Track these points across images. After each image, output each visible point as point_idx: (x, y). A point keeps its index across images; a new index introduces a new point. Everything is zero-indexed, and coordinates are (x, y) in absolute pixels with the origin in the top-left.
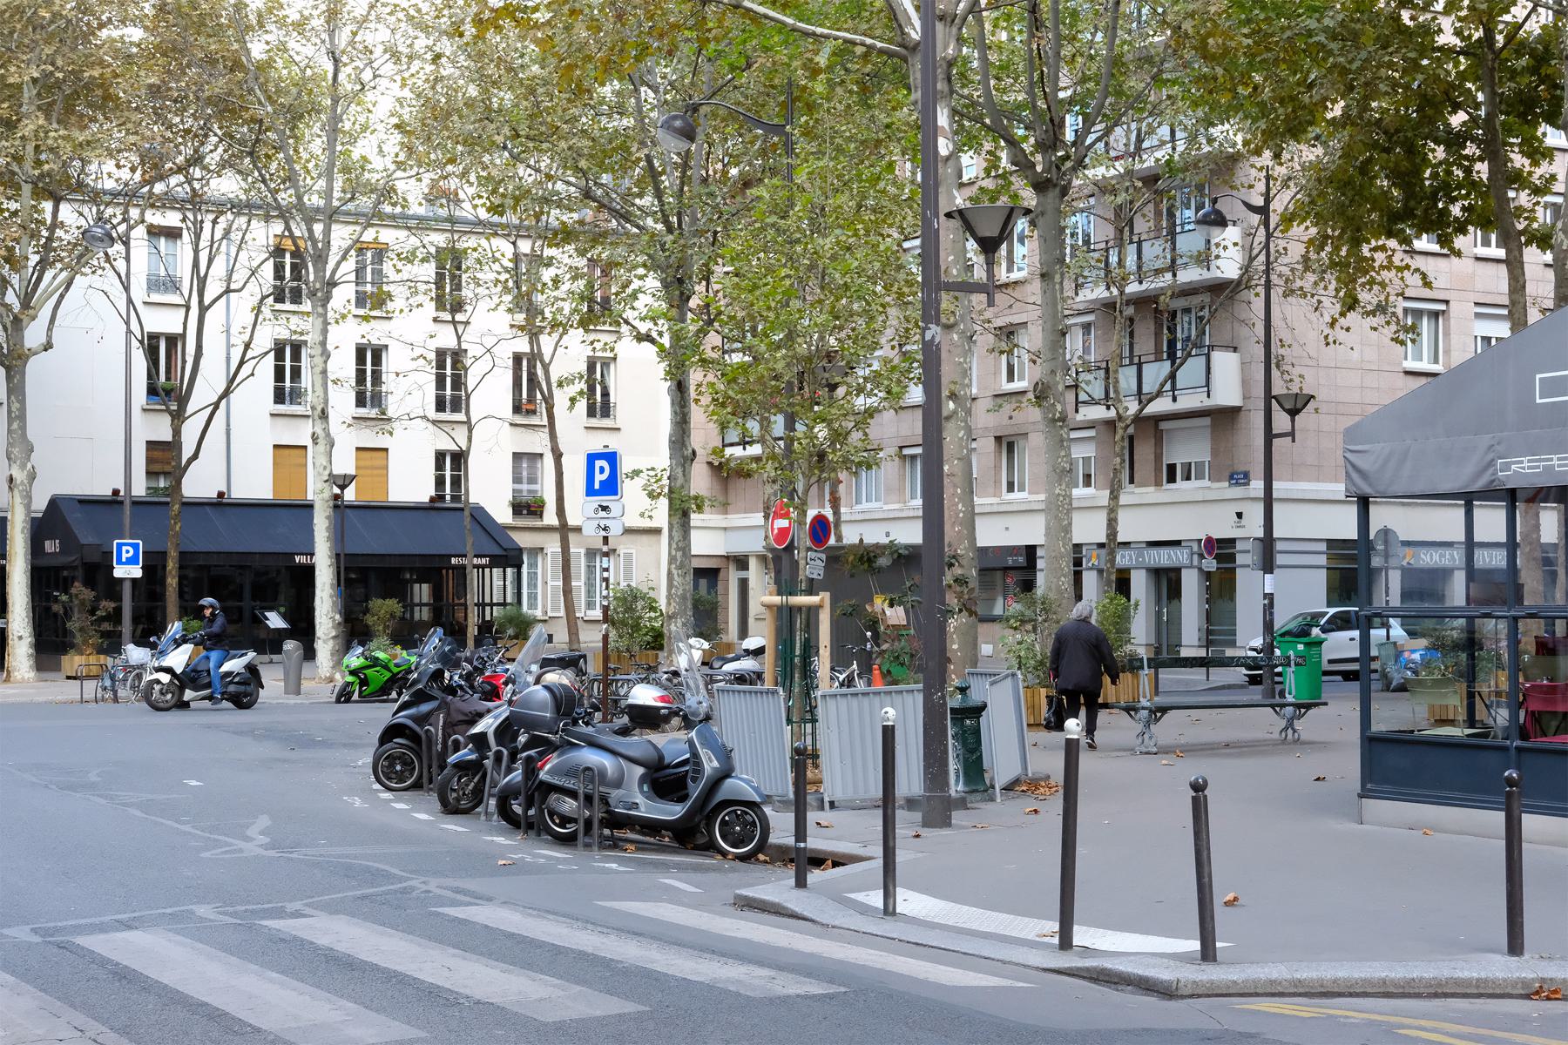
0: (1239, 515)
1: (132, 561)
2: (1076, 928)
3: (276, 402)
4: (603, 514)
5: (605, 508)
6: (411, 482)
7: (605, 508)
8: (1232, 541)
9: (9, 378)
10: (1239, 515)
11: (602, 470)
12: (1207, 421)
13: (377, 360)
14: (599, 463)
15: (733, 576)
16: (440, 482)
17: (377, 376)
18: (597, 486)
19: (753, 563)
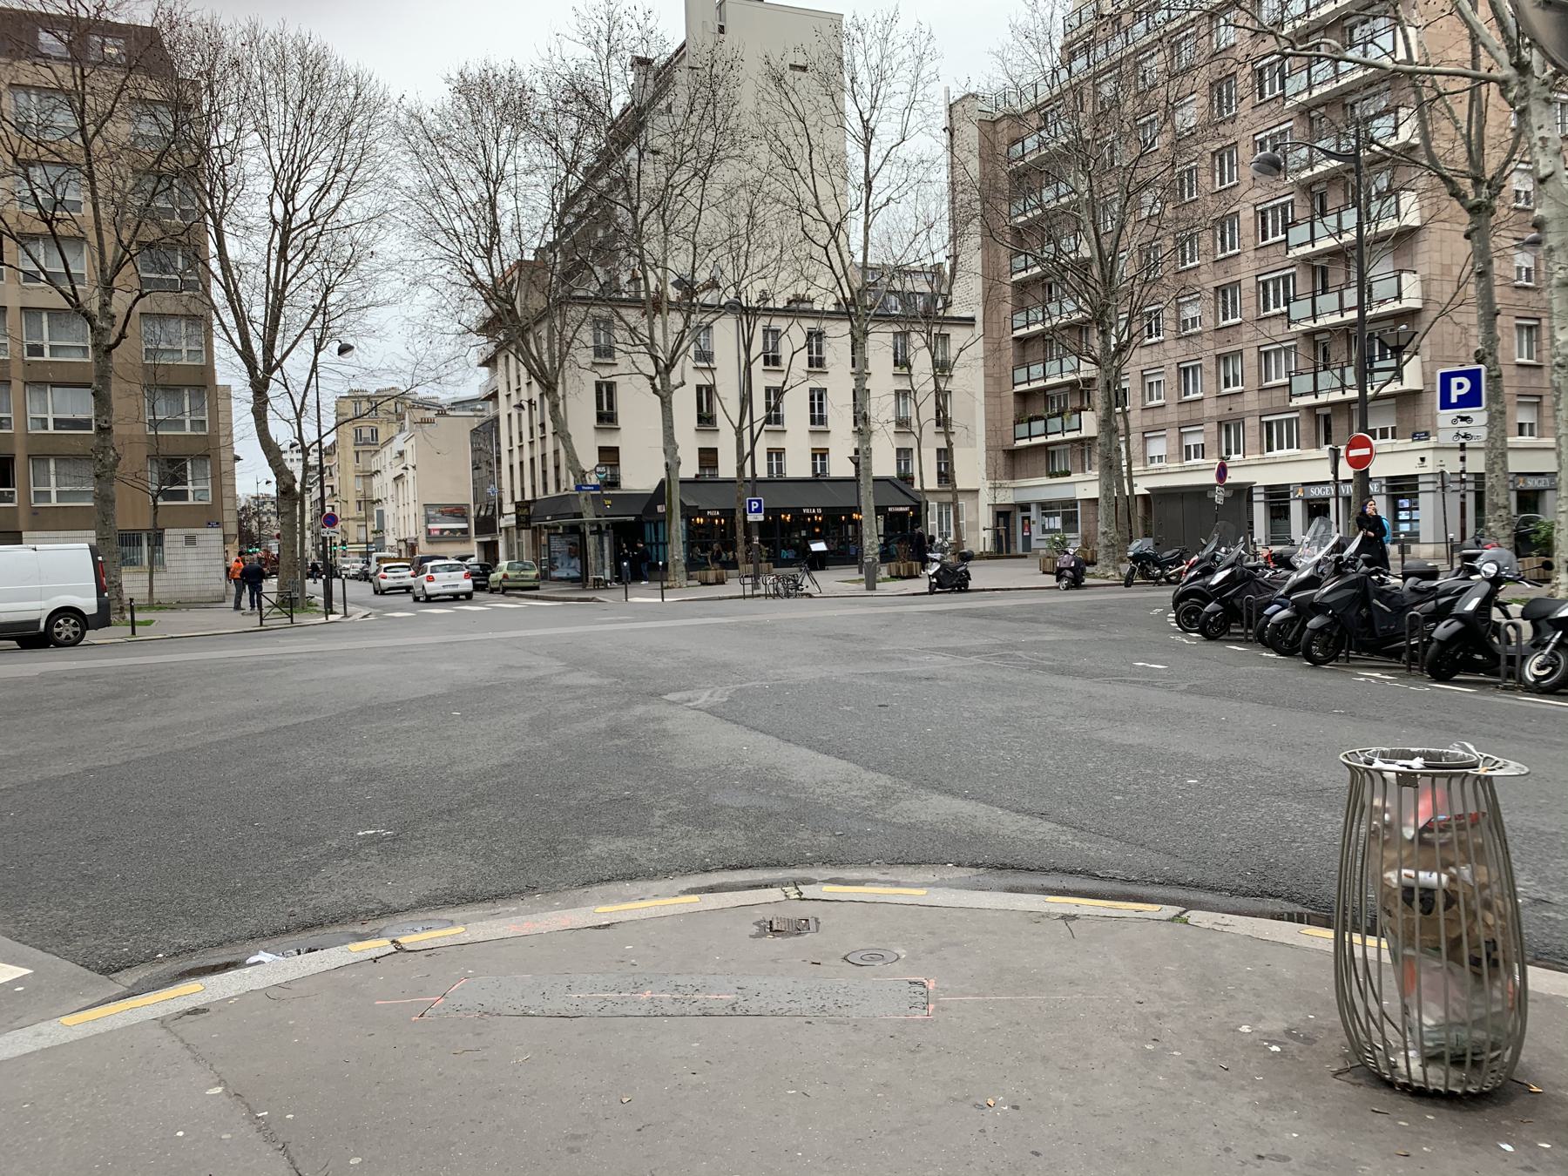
0: (1423, 459)
1: (758, 511)
2: (1331, 949)
3: (616, 449)
4: (1464, 424)
5: (1463, 419)
6: (798, 466)
7: (1463, 419)
8: (1416, 476)
9: (663, 403)
10: (1423, 459)
11: (1460, 386)
12: (1393, 401)
13: (820, 398)
14: (1454, 381)
15: (1019, 515)
16: (814, 465)
17: (821, 406)
18: (1454, 400)
19: (1033, 508)
